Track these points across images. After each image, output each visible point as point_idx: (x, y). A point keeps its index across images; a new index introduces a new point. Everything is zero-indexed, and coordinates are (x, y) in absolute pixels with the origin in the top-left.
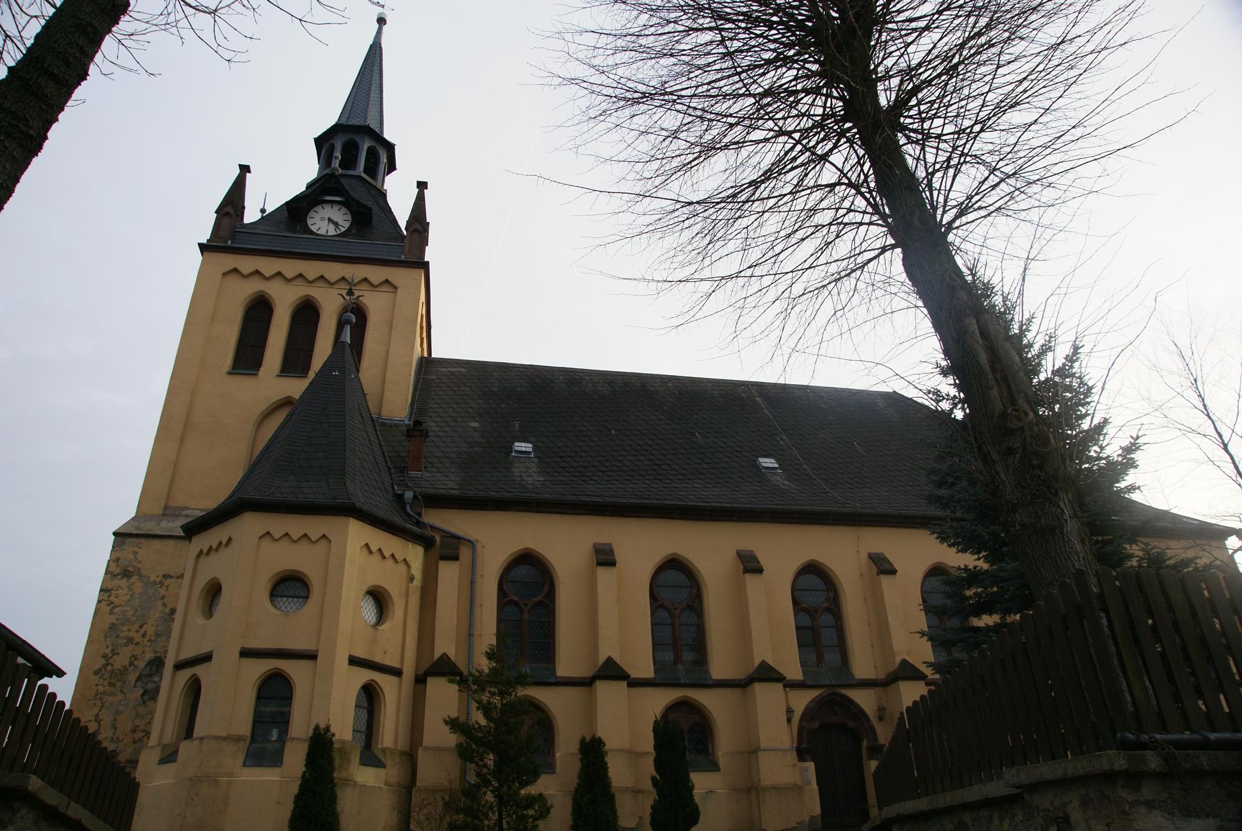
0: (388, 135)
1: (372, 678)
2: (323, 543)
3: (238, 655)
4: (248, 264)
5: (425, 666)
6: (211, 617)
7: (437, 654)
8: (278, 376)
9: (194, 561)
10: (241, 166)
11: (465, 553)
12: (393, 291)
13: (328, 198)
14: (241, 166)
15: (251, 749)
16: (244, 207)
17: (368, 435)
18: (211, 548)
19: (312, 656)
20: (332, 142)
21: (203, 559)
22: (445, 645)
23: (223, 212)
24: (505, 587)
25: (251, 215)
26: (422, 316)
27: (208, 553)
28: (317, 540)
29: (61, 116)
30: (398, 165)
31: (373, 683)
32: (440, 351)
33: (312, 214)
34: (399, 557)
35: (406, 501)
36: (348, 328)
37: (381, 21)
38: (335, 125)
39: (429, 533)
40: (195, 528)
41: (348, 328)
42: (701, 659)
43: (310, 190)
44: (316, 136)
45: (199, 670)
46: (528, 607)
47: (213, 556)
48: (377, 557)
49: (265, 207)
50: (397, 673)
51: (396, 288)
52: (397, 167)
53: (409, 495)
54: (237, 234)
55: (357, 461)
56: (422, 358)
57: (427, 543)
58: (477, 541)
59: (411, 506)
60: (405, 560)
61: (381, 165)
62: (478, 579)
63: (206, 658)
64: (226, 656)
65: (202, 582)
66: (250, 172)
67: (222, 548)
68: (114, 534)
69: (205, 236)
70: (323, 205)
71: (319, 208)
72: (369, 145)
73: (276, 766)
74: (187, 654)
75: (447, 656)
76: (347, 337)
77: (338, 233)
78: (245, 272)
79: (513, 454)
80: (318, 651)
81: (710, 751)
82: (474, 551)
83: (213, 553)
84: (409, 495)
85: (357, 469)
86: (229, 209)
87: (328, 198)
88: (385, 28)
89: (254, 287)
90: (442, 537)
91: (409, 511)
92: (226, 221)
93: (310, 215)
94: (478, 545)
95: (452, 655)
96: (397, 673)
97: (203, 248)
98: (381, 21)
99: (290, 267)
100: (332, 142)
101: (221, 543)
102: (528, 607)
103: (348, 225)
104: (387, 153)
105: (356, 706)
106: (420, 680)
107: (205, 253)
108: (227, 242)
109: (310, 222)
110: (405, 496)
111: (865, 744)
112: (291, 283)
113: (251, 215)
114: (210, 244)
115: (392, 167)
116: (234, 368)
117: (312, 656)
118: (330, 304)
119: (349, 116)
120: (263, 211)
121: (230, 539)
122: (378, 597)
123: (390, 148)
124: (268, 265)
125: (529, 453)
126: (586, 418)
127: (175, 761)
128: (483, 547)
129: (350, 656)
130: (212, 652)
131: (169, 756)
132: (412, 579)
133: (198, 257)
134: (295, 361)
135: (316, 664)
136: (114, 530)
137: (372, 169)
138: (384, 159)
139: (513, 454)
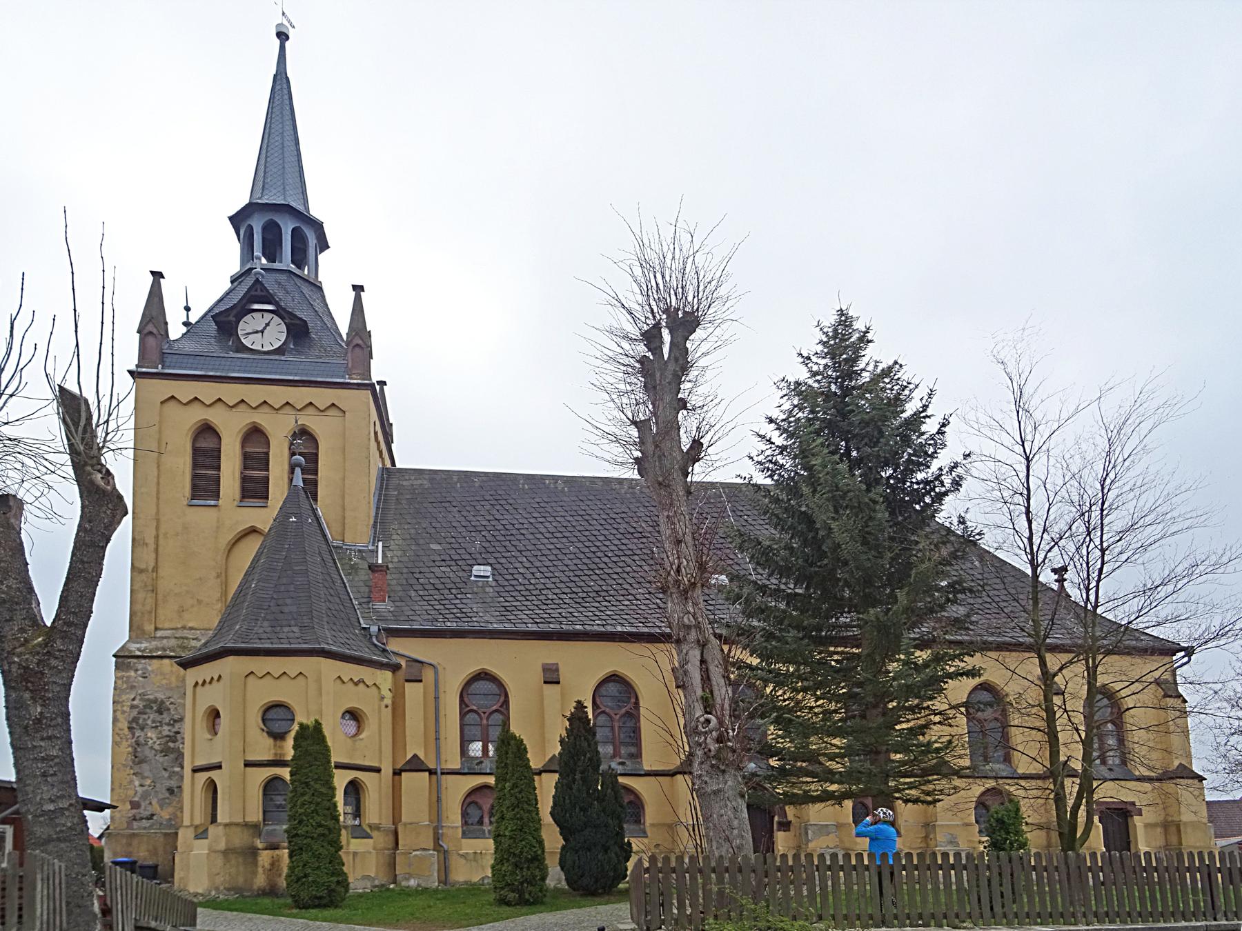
0: (315, 211)
6: (216, 734)
9: (192, 689)
10: (153, 273)
11: (428, 675)
13: (256, 306)
14: (153, 273)
16: (166, 323)
17: (331, 577)
20: (249, 223)
22: (415, 748)
23: (145, 331)
24: (466, 699)
26: (376, 433)
30: (330, 242)
32: (403, 461)
36: (298, 470)
37: (282, 36)
39: (395, 660)
41: (298, 470)
42: (637, 756)
45: (213, 774)
46: (486, 715)
48: (351, 685)
51: (344, 412)
52: (330, 245)
53: (374, 629)
54: (166, 355)
55: (323, 604)
56: (384, 469)
57: (395, 668)
59: (377, 637)
60: (375, 684)
61: (310, 249)
62: (442, 696)
63: (219, 767)
65: (202, 709)
66: (163, 278)
71: (248, 318)
72: (293, 226)
74: (200, 762)
76: (299, 480)
79: (473, 578)
81: (642, 821)
82: (436, 673)
84: (374, 629)
85: (324, 612)
86: (150, 328)
87: (256, 306)
88: (288, 44)
89: (197, 415)
90: (407, 661)
91: (376, 642)
92: (151, 341)
93: (245, 319)
95: (422, 756)
98: (282, 36)
100: (249, 223)
101: (212, 678)
102: (486, 715)
106: (397, 773)
111: (776, 819)
112: (234, 410)
113: (176, 331)
115: (323, 245)
116: (194, 497)
118: (279, 430)
119: (263, 186)
122: (354, 715)
123: (318, 226)
124: (208, 391)
125: (488, 577)
132: (382, 698)
134: (254, 490)
137: (300, 256)
138: (312, 241)
139: (473, 578)
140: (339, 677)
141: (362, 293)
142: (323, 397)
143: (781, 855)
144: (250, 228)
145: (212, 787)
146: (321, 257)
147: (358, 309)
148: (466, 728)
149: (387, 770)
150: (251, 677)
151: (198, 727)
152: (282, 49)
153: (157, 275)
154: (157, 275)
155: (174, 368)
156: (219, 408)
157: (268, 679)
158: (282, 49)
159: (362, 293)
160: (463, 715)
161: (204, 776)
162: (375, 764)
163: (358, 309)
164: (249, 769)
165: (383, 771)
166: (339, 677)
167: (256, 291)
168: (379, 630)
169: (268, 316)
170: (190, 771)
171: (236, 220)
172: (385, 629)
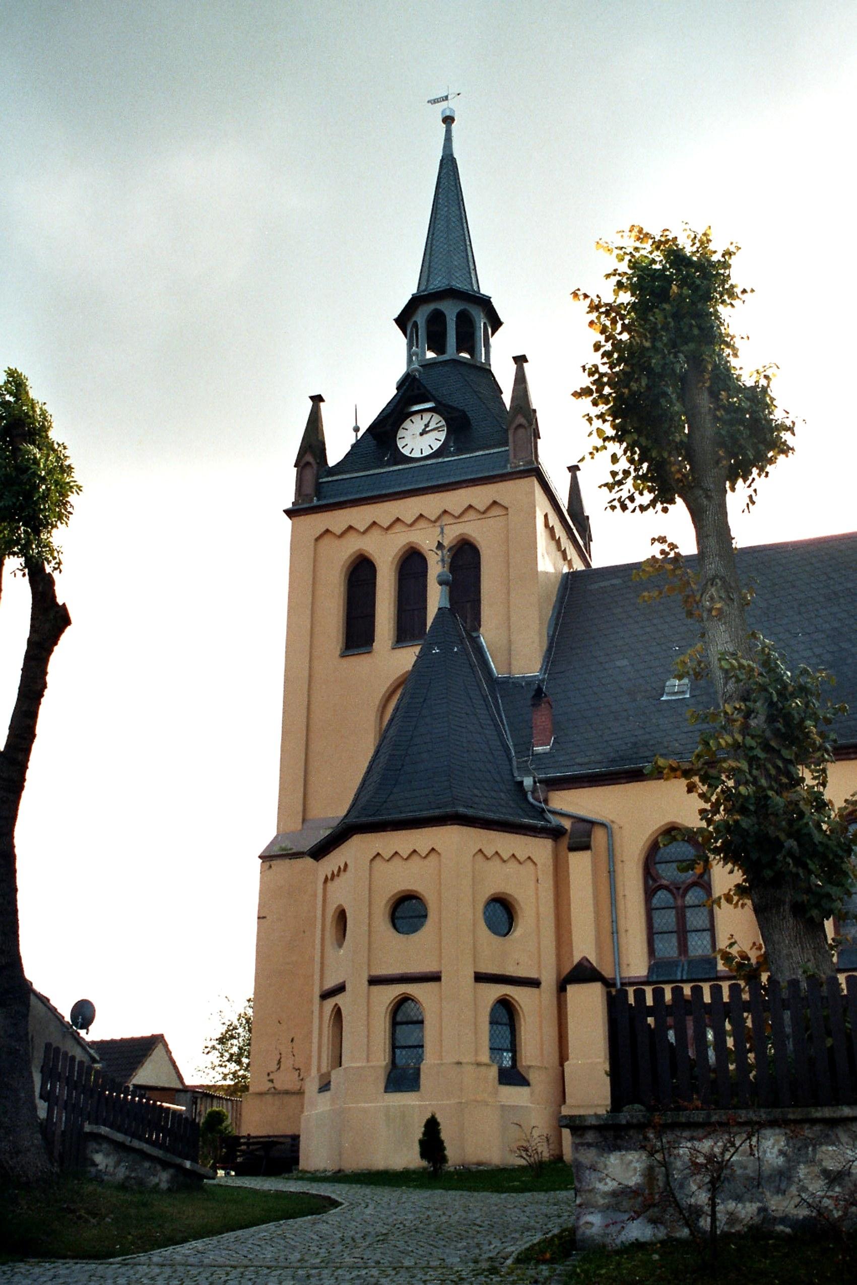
1: (505, 993)
2: (433, 856)
3: (367, 983)
4: (338, 520)
5: (567, 969)
7: (576, 959)
8: (393, 649)
10: (312, 398)
11: (599, 837)
12: (505, 513)
14: (312, 398)
15: (392, 1075)
18: (333, 873)
19: (435, 978)
21: (329, 884)
23: (302, 464)
25: (335, 453)
27: (332, 879)
28: (427, 855)
29: (49, 679)
31: (507, 998)
33: (401, 433)
34: (521, 856)
35: (526, 788)
38: (411, 299)
40: (319, 852)
43: (402, 391)
44: (396, 316)
45: (338, 999)
46: (681, 891)
47: (337, 881)
49: (358, 425)
50: (534, 983)
51: (507, 509)
52: (502, 320)
54: (323, 485)
57: (556, 833)
58: (613, 822)
63: (340, 989)
64: (357, 985)
66: (579, 470)
67: (342, 873)
68: (260, 857)
69: (288, 499)
70: (402, 426)
71: (407, 424)
73: (415, 1091)
74: (330, 984)
75: (587, 960)
77: (445, 429)
78: (338, 530)
80: (441, 972)
82: (610, 835)
83: (336, 878)
93: (399, 436)
94: (615, 826)
96: (534, 983)
97: (289, 513)
99: (384, 512)
101: (340, 868)
103: (444, 436)
104: (483, 312)
105: (491, 1023)
106: (562, 989)
107: (293, 518)
108: (312, 501)
109: (400, 444)
110: (525, 784)
113: (335, 453)
114: (296, 508)
115: (496, 323)
117: (435, 978)
120: (356, 429)
121: (346, 865)
123: (485, 304)
125: (683, 692)
126: (450, 799)
127: (329, 1090)
128: (621, 828)
129: (475, 973)
130: (345, 982)
131: (325, 1087)
133: (287, 522)
135: (440, 987)
136: (259, 854)
137: (467, 340)
138: (481, 322)
140: (480, 850)
141: (525, 365)
142: (480, 496)
143: (54, 1049)
144: (415, 325)
145: (338, 1013)
146: (492, 340)
147: (520, 380)
148: (656, 915)
149: (549, 979)
150: (378, 859)
151: (328, 935)
152: (448, 133)
153: (317, 399)
154: (317, 399)
155: (335, 496)
156: (375, 533)
157: (396, 861)
158: (448, 133)
159: (525, 365)
160: (649, 893)
161: (330, 1003)
162: (533, 975)
163: (520, 380)
164: (375, 989)
165: (543, 985)
166: (480, 850)
167: (413, 391)
168: (535, 782)
169: (427, 416)
170: (318, 998)
171: (402, 321)
172: (540, 781)
